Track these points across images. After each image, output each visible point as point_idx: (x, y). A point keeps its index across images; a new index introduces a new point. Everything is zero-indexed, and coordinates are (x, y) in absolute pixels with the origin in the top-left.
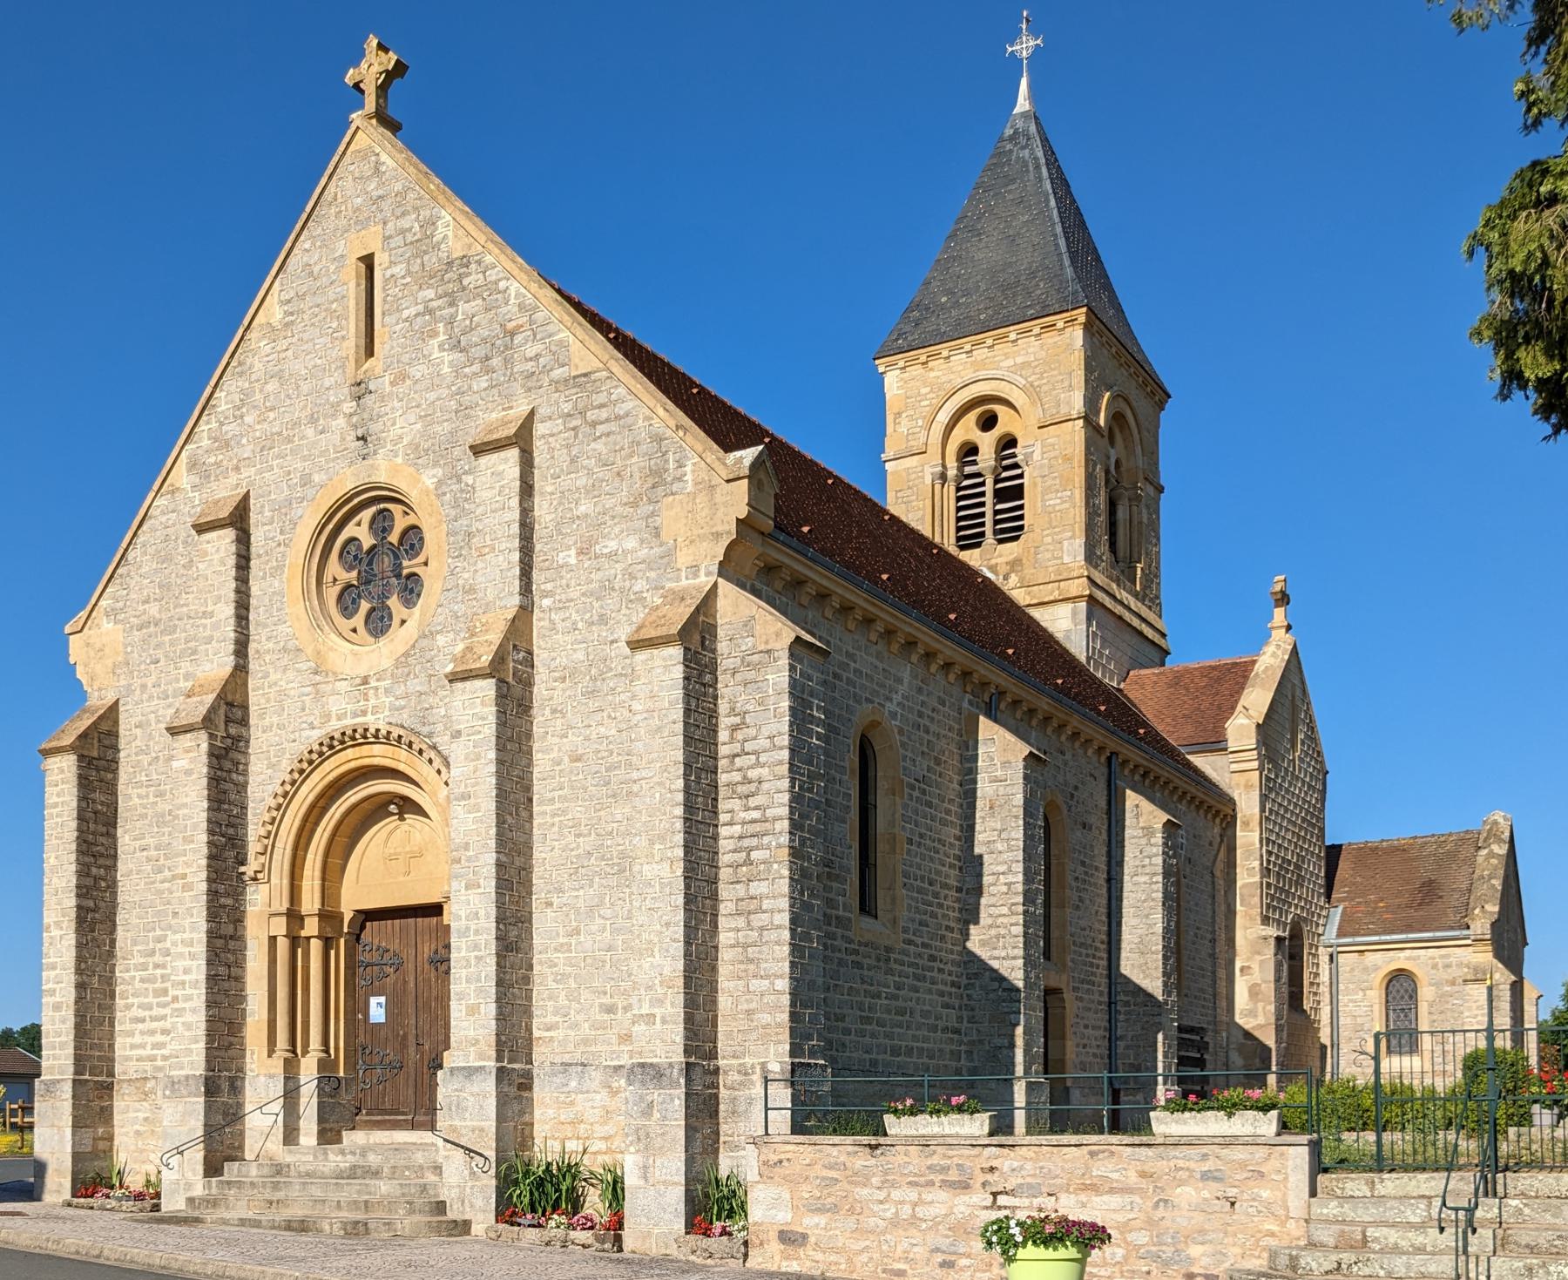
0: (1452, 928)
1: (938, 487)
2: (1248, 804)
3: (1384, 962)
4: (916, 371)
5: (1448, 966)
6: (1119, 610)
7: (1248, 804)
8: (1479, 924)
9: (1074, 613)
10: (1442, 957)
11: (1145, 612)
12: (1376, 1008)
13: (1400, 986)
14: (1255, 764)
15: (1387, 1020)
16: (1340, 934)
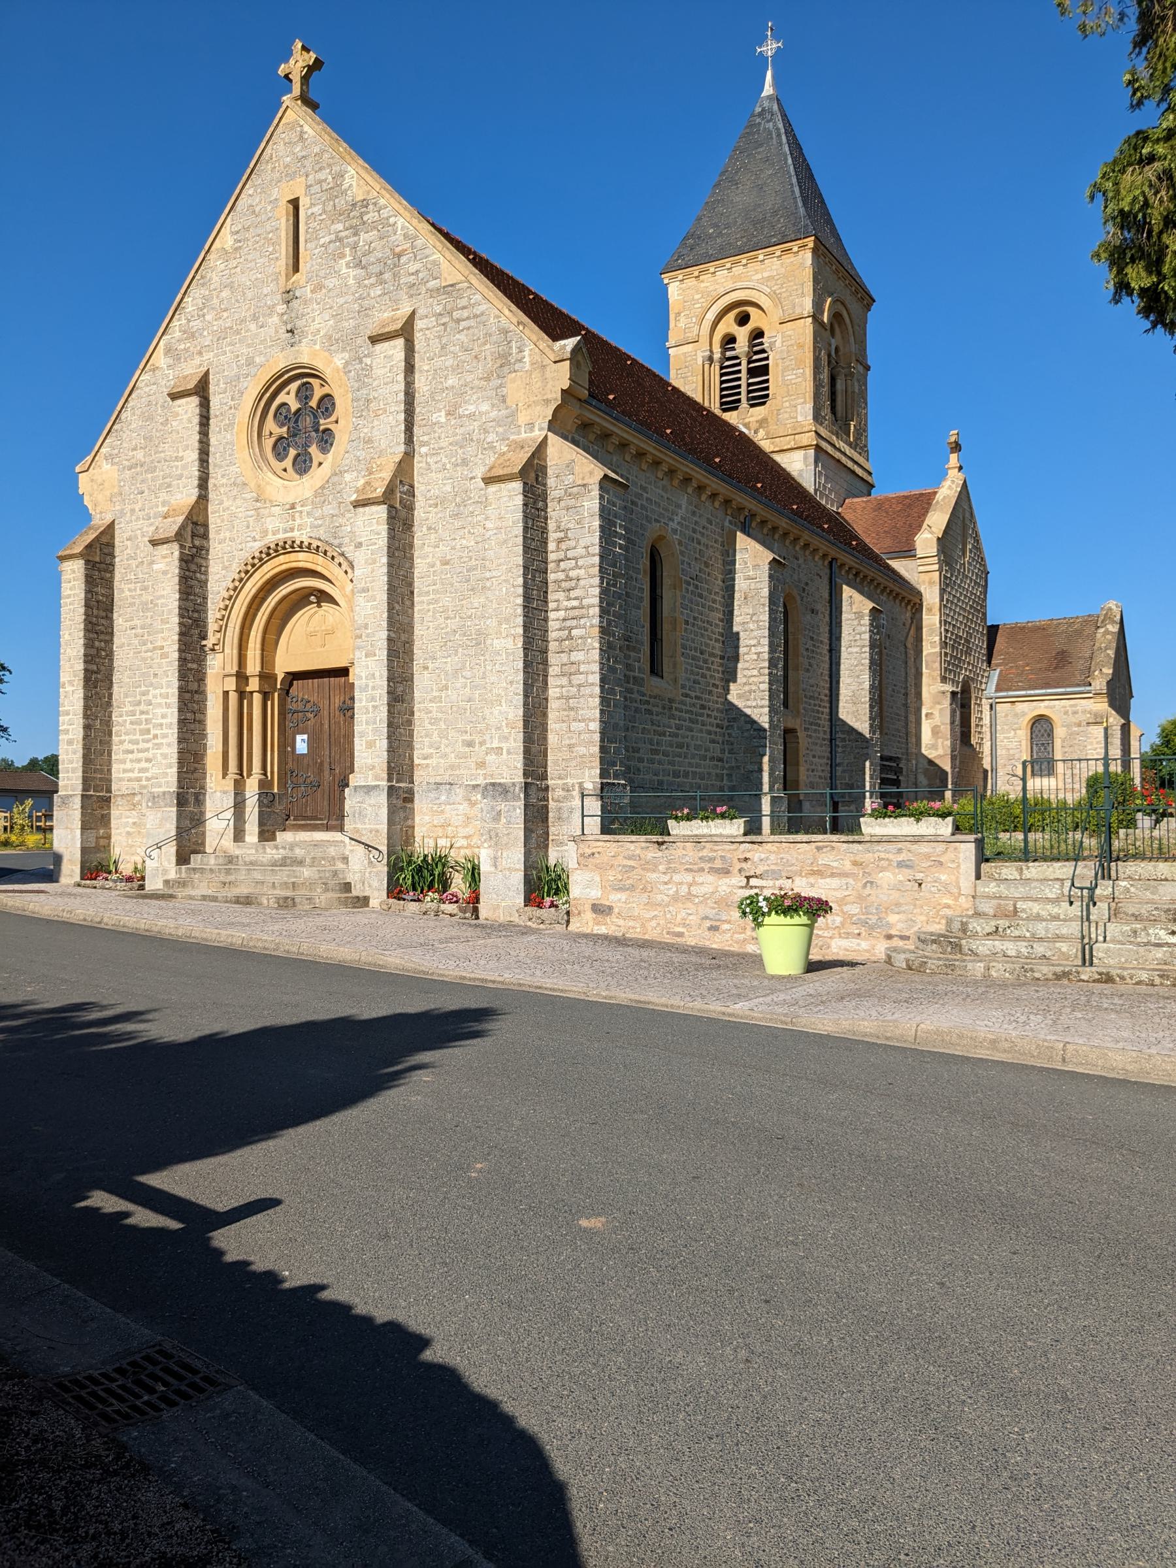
1: (707, 366)
2: (931, 596)
5: (1075, 713)
6: (837, 455)
7: (931, 596)
9: (805, 458)
10: (1071, 706)
12: (1024, 743)
13: (1041, 728)
14: (936, 567)
15: (1032, 752)
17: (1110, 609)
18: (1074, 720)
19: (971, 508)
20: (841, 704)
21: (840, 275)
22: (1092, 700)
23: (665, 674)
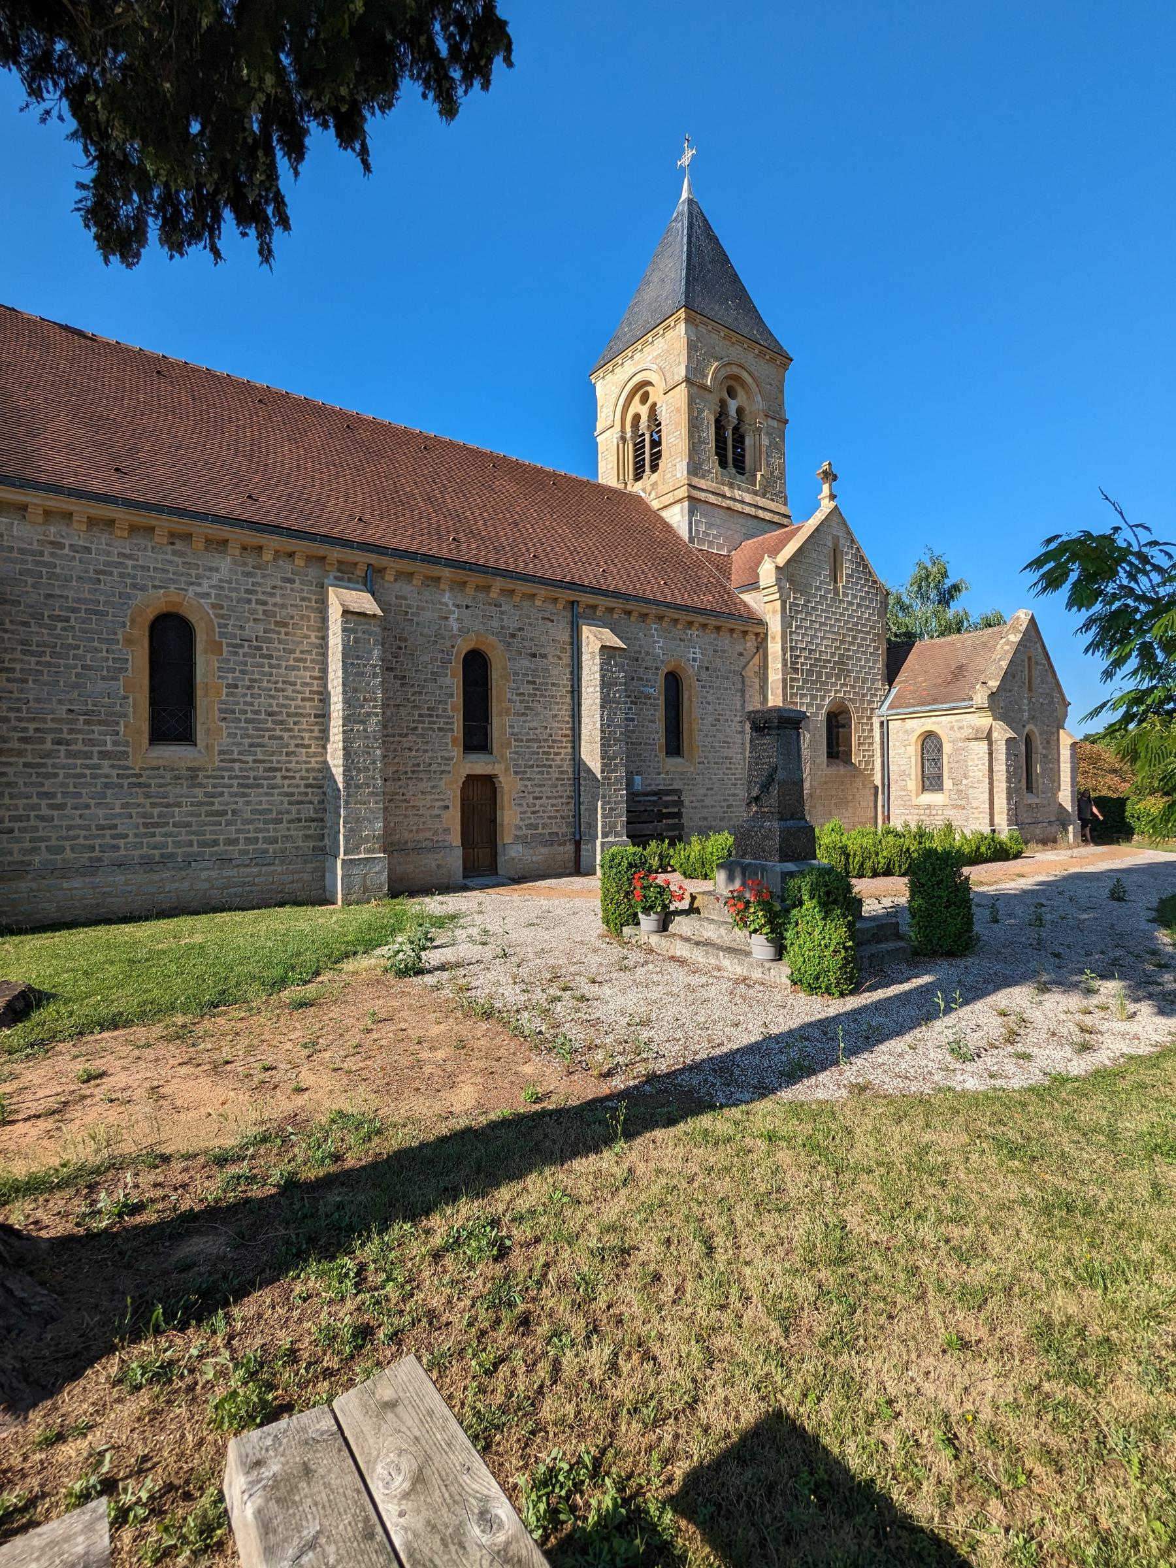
0: (913, 706)
1: (621, 446)
2: (775, 625)
3: (919, 726)
4: (609, 377)
5: (961, 728)
6: (726, 503)
7: (775, 625)
8: (979, 696)
9: (682, 510)
10: (957, 721)
11: (772, 505)
12: (913, 759)
13: (930, 743)
14: (777, 596)
15: (923, 767)
16: (889, 709)
17: (1018, 618)
18: (959, 735)
19: (849, 533)
20: (583, 744)
21: (734, 340)
22: (976, 715)
23: (198, 742)
